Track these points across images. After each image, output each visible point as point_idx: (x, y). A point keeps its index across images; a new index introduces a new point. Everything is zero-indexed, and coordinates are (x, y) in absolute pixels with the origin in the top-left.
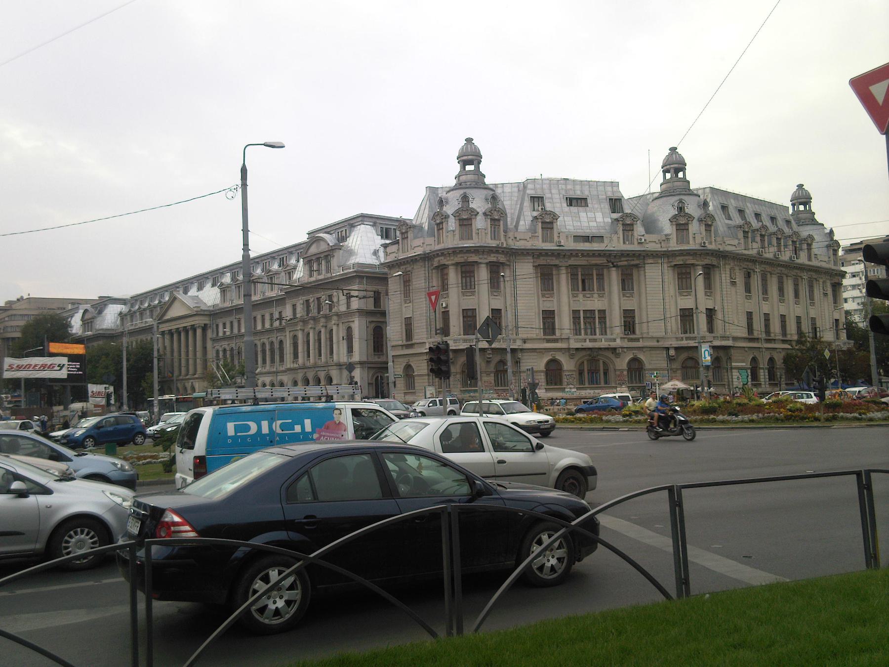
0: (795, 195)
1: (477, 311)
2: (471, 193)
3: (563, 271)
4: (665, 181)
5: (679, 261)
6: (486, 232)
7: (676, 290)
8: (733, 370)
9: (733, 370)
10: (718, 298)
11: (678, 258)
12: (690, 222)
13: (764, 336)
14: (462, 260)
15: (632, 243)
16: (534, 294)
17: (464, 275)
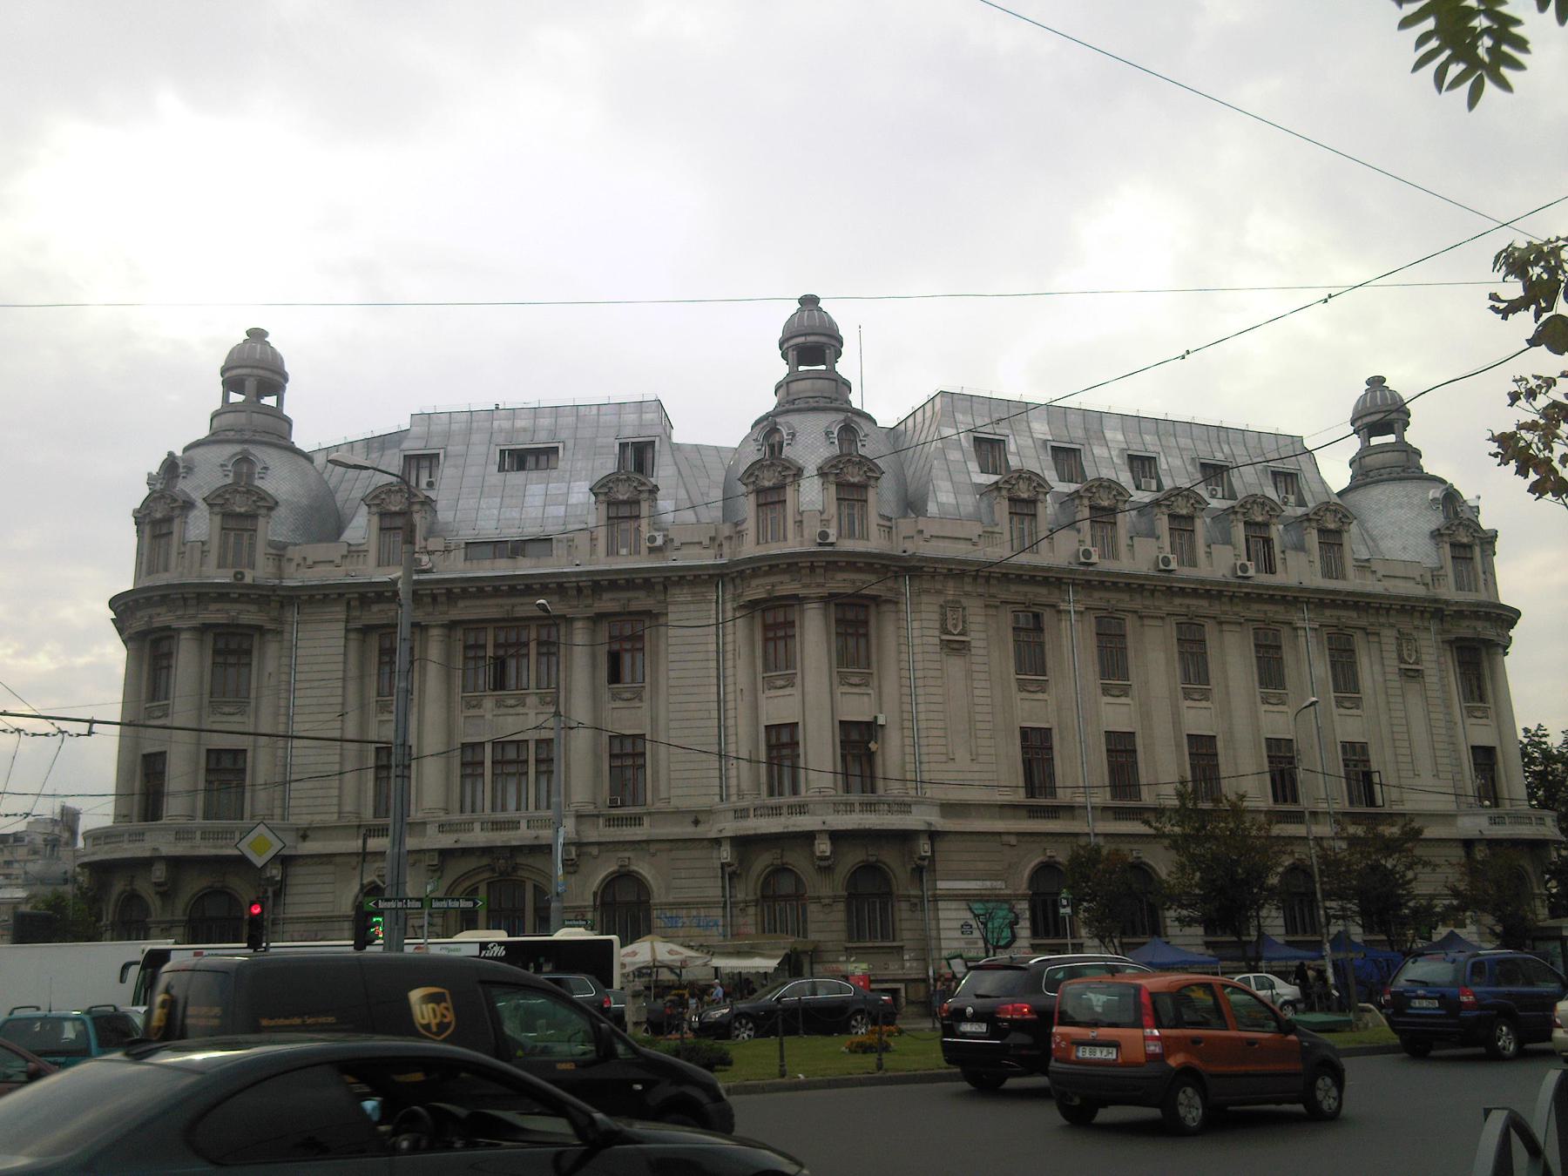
1: (249, 754)
3: (580, 635)
5: (757, 590)
7: (830, 668)
10: (890, 687)
11: (840, 576)
12: (872, 482)
15: (636, 551)
16: (669, 687)
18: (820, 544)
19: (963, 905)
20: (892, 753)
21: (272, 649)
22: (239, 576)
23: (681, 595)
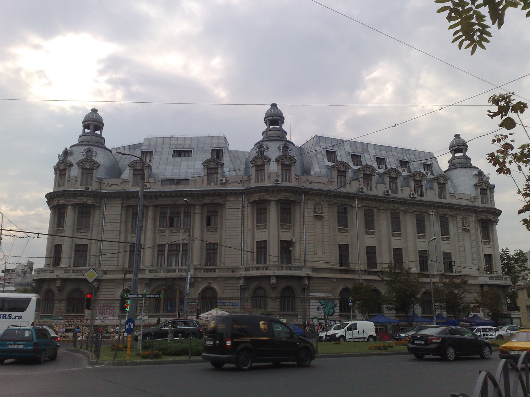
0: (453, 142)
2: (95, 149)
3: (198, 210)
4: (84, 134)
5: (255, 198)
6: (76, 179)
8: (311, 301)
9: (311, 301)
10: (297, 230)
13: (364, 268)
14: (81, 202)
17: (186, 215)
18: (276, 183)
19: (318, 301)
20: (297, 251)
21: (97, 212)
22: (87, 188)
23: (231, 199)
